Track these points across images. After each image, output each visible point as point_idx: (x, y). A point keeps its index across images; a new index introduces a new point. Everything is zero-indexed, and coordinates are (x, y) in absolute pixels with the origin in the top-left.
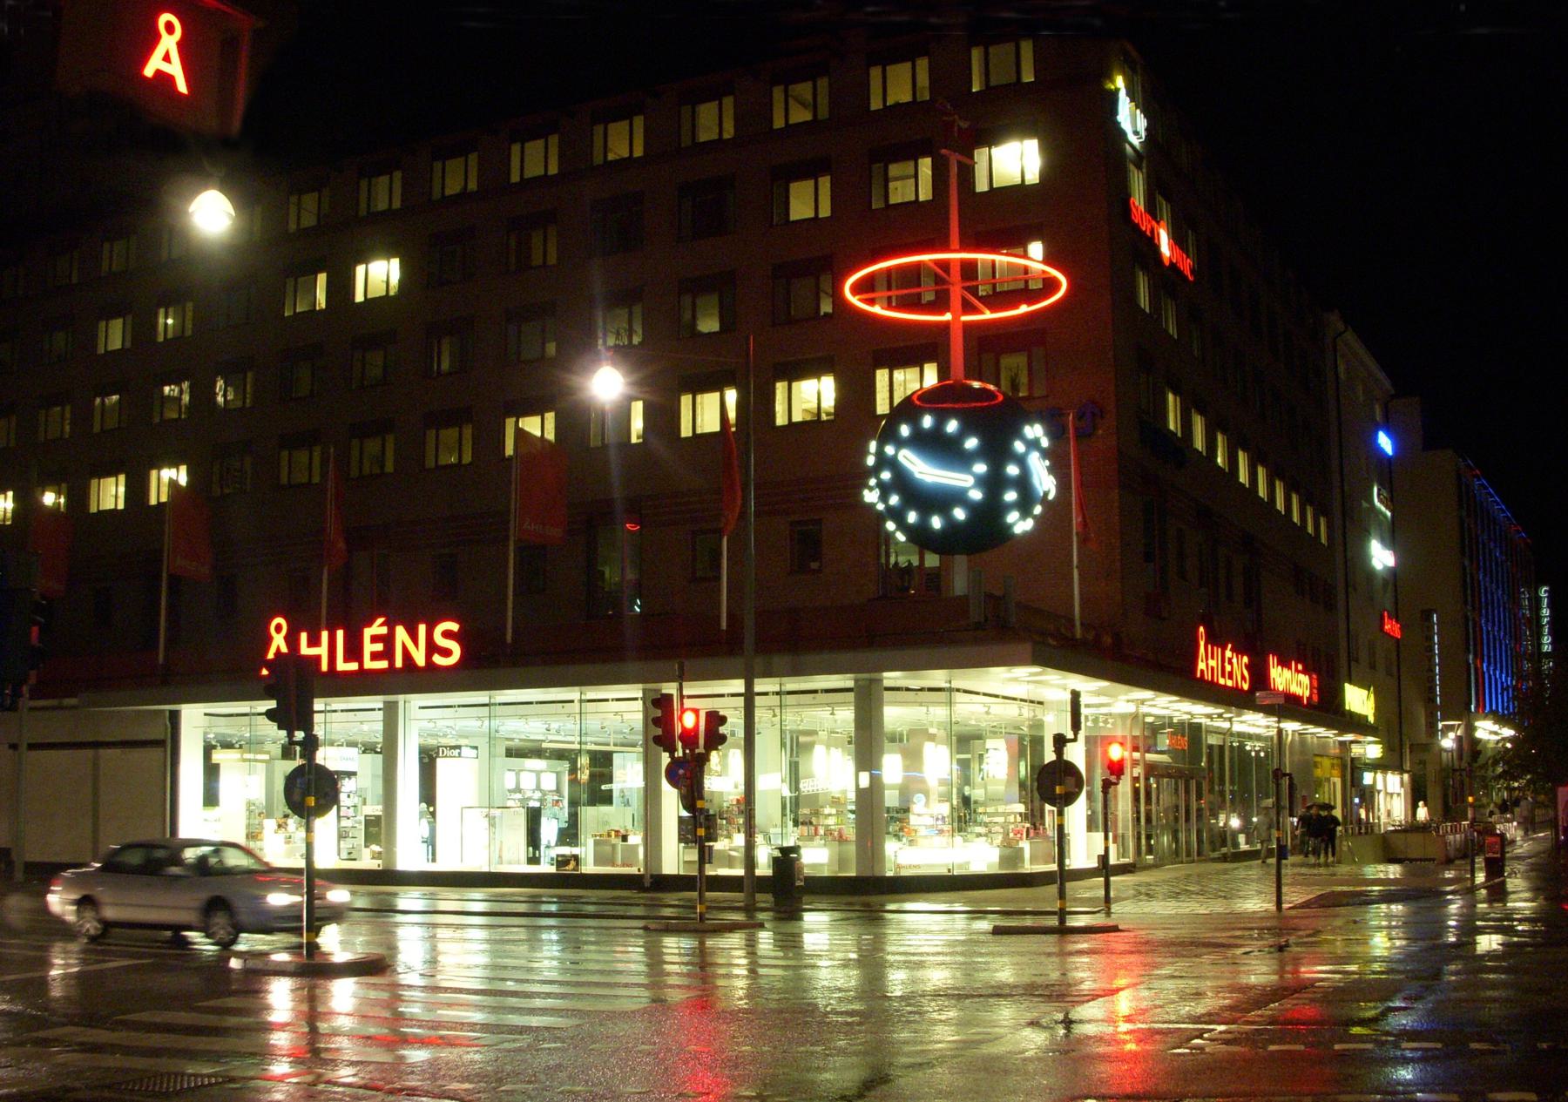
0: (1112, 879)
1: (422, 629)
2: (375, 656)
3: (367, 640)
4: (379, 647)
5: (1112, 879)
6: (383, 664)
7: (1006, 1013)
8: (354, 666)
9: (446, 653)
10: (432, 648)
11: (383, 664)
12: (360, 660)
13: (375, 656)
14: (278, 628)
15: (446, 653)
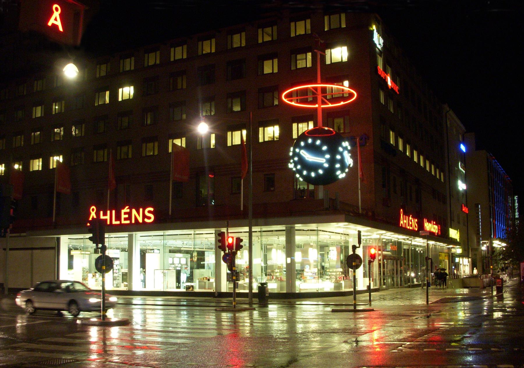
0: (372, 293)
1: (141, 210)
2: (125, 219)
3: (123, 214)
4: (127, 216)
5: (372, 293)
6: (128, 222)
7: (336, 338)
8: (118, 222)
9: (149, 218)
10: (144, 216)
11: (128, 222)
12: (120, 220)
13: (125, 219)
14: (93, 210)
15: (149, 218)
